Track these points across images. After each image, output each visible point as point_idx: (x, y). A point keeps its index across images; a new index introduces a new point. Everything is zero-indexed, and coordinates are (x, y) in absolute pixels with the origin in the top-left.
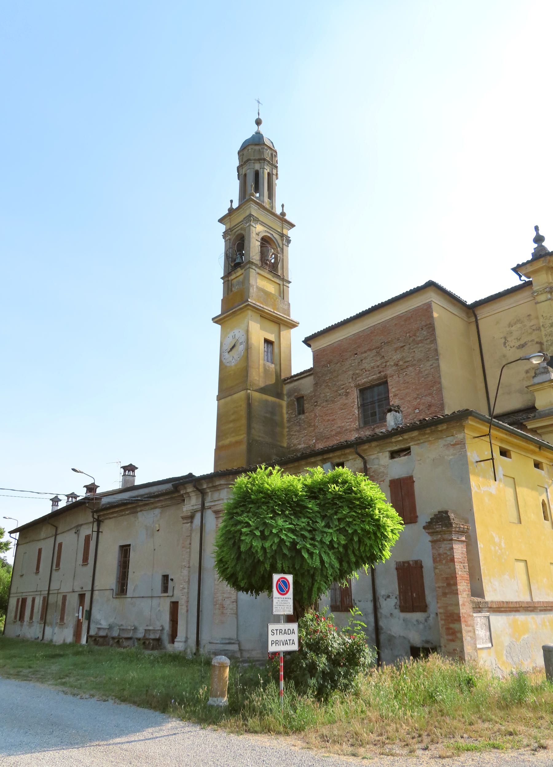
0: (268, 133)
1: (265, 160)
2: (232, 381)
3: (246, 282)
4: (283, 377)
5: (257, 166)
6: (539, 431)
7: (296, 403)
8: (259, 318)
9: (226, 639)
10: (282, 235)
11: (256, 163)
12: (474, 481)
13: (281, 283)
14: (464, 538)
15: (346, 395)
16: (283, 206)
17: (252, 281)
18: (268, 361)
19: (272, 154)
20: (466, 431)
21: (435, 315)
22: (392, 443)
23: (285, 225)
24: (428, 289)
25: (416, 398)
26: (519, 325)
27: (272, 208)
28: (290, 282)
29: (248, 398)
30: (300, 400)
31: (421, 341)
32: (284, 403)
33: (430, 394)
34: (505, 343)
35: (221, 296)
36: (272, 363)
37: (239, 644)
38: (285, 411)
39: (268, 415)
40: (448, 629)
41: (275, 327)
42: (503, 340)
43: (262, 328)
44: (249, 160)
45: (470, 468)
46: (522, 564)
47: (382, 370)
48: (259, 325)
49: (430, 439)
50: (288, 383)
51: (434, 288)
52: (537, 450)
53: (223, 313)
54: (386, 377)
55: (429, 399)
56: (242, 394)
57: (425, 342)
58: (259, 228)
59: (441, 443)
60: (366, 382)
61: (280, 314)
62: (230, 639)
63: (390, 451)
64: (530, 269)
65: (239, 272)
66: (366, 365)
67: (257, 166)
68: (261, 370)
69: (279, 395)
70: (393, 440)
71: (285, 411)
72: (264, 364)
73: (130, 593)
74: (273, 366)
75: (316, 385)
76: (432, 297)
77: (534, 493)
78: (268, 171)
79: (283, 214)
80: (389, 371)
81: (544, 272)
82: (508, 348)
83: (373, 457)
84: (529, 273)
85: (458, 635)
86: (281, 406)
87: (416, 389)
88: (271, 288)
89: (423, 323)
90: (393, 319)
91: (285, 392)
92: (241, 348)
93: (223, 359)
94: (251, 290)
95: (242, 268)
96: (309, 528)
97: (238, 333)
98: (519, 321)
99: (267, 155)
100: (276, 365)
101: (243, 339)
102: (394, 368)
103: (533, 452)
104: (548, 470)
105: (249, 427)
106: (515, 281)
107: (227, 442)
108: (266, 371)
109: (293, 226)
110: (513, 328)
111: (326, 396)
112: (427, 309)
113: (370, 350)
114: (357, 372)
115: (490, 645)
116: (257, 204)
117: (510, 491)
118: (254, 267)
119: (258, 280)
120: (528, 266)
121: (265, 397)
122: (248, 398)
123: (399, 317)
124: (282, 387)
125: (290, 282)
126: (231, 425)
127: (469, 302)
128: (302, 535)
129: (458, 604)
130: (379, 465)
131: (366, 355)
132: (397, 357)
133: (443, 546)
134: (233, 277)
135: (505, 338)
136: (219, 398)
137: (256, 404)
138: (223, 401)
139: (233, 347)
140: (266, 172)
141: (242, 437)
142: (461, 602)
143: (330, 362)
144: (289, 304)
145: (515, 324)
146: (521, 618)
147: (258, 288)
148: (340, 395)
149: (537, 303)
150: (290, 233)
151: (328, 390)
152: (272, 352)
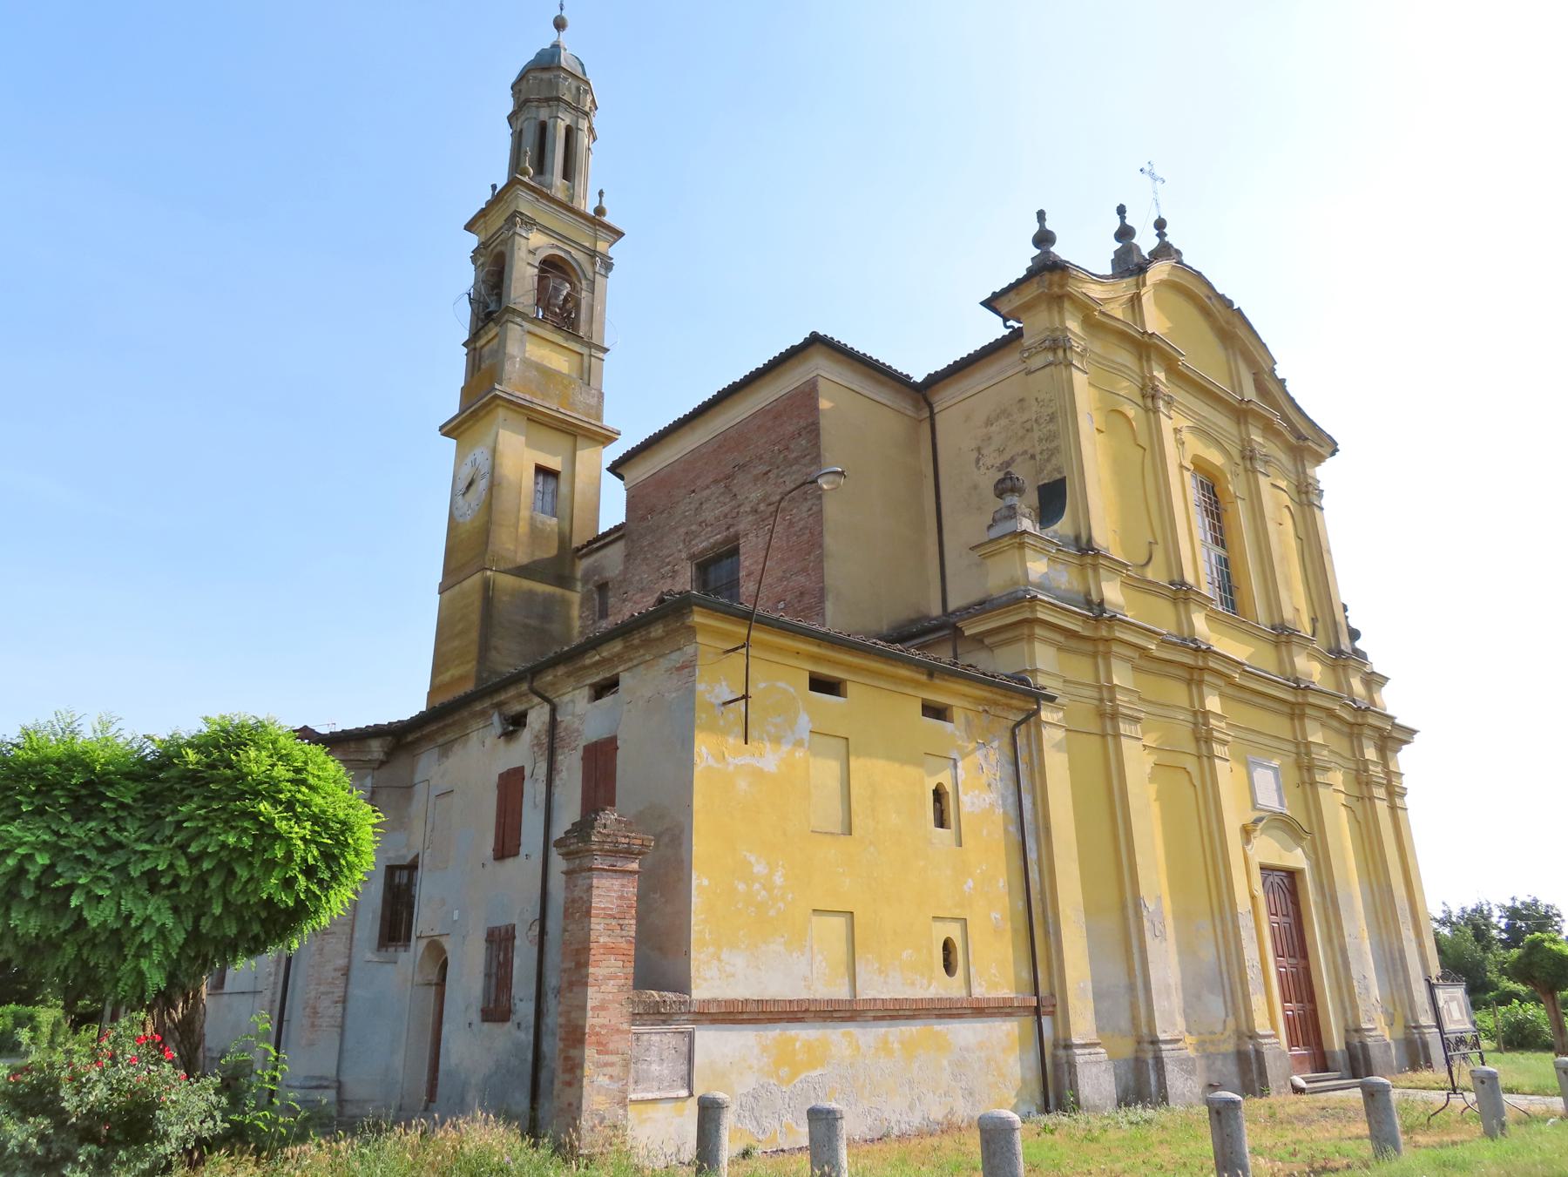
0: (573, 47)
1: (558, 99)
2: (467, 551)
3: (500, 352)
4: (577, 542)
5: (544, 114)
6: (987, 641)
7: (596, 596)
8: (525, 422)
9: (313, 1078)
10: (592, 254)
11: (547, 105)
12: (704, 747)
13: (585, 351)
14: (635, 866)
15: (673, 577)
16: (601, 194)
17: (512, 348)
18: (543, 512)
19: (578, 89)
20: (699, 639)
21: (824, 404)
22: (585, 667)
23: (602, 233)
24: (812, 349)
25: (781, 579)
26: (1003, 422)
27: (572, 198)
28: (606, 350)
29: (487, 586)
30: (603, 587)
31: (797, 460)
32: (575, 597)
33: (804, 570)
34: (978, 460)
35: (460, 382)
36: (554, 515)
37: (340, 1087)
38: (575, 612)
39: (533, 622)
40: (567, 1058)
41: (564, 442)
42: (975, 454)
43: (530, 444)
44: (527, 101)
45: (701, 717)
46: (840, 923)
47: (730, 521)
48: (523, 439)
49: (647, 657)
50: (585, 555)
51: (824, 349)
52: (924, 678)
53: (462, 411)
54: (737, 537)
55: (802, 579)
56: (478, 577)
57: (804, 461)
58: (536, 239)
59: (664, 663)
60: (705, 549)
61: (576, 415)
62: (321, 1078)
63: (592, 685)
64: (1015, 301)
65: (493, 330)
66: (708, 516)
67: (544, 114)
68: (523, 528)
69: (564, 581)
70: (588, 662)
71: (575, 612)
72: (532, 518)
73: (227, 988)
74: (555, 520)
75: (628, 556)
76: (820, 366)
77: (911, 772)
78: (568, 122)
79: (600, 211)
80: (741, 527)
81: (1044, 306)
82: (983, 470)
83: (566, 698)
84: (1017, 308)
85: (578, 1072)
86: (566, 603)
87: (782, 559)
88: (560, 362)
89: (803, 423)
90: (754, 415)
91: (579, 574)
92: (482, 485)
93: (456, 513)
94: (508, 367)
95: (497, 322)
96: (101, 843)
97: (480, 454)
98: (1004, 413)
99: (566, 91)
100: (560, 519)
101: (485, 469)
102: (750, 518)
103: (917, 684)
104: (968, 723)
105: (485, 647)
106: (993, 328)
107: (446, 677)
108: (536, 533)
109: (620, 234)
110: (994, 428)
111: (641, 580)
112: (808, 395)
113: (716, 482)
114: (693, 527)
115: (684, 1093)
116: (533, 189)
117: (832, 767)
118: (518, 320)
119: (528, 347)
120: (1012, 295)
121: (527, 584)
122: (487, 586)
123: (763, 412)
124: (573, 565)
125: (606, 350)
126: (456, 643)
127: (918, 377)
128: (82, 857)
129: (584, 1008)
130: (573, 715)
131: (708, 492)
132: (756, 495)
133: (580, 882)
134: (483, 341)
135: (979, 449)
136: (443, 589)
137: (505, 598)
138: (447, 594)
139: (470, 484)
140: (561, 126)
141: (469, 666)
142: (590, 1004)
143: (652, 511)
144: (601, 395)
145: (998, 418)
146: (803, 1035)
147: (527, 363)
148: (663, 577)
149: (1029, 373)
150: (616, 252)
151: (645, 567)
152: (555, 494)
